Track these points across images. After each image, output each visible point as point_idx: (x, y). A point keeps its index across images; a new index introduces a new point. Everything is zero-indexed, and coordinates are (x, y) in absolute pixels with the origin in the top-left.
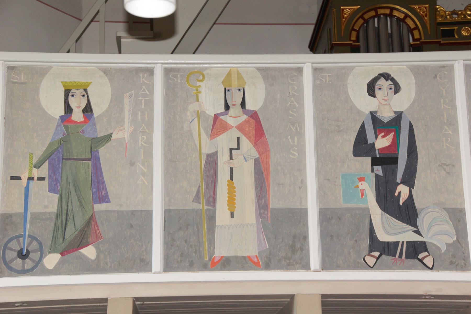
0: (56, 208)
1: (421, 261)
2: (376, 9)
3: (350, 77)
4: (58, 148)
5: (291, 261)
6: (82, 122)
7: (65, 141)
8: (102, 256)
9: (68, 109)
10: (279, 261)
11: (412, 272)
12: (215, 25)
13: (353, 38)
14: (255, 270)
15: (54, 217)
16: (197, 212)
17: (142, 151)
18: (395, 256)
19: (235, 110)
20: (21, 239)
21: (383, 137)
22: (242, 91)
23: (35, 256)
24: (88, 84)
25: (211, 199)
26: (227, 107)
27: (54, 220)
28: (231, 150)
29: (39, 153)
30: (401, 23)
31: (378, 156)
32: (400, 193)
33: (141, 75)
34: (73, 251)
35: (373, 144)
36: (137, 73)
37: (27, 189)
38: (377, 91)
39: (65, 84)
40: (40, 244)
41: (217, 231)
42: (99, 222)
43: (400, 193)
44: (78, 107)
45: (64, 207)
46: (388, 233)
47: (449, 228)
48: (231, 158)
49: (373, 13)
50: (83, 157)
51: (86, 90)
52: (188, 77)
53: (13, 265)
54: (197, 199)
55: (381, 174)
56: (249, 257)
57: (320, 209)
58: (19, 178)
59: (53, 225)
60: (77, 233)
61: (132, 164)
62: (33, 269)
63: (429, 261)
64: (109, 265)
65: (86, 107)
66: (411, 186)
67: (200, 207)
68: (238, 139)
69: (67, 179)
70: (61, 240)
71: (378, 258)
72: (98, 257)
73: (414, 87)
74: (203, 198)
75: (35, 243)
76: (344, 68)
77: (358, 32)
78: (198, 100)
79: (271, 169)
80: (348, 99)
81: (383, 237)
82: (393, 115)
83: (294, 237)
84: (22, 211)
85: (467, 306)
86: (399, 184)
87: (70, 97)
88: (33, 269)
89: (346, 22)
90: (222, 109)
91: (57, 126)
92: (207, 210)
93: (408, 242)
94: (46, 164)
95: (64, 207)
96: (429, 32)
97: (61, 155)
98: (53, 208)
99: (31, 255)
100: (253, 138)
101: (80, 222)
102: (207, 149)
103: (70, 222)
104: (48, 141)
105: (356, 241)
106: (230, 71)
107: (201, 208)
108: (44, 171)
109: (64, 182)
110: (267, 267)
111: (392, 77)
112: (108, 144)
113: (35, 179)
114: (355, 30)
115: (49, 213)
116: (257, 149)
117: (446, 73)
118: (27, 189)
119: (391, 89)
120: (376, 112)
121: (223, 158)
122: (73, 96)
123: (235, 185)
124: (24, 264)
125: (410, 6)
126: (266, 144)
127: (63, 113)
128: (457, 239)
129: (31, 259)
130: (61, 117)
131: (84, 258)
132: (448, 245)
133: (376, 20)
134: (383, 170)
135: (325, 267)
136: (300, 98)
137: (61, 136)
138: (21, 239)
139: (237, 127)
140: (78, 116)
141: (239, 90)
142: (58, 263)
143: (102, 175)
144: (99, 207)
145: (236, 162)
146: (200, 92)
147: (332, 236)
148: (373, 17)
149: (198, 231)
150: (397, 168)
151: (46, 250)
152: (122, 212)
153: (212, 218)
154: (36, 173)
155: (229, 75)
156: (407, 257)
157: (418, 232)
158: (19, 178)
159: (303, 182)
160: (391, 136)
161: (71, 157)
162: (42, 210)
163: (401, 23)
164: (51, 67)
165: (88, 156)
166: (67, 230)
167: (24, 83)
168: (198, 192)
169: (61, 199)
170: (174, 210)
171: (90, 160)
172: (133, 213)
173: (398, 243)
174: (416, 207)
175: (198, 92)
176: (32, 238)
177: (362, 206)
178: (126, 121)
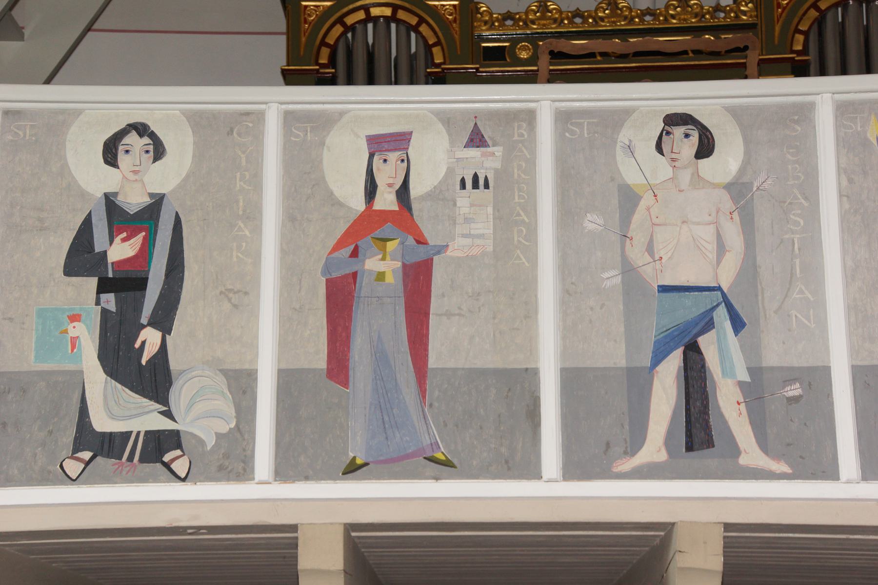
1: (167, 466)
18: (120, 458)
21: (124, 240)
22: (406, 161)
32: (143, 343)
35: (105, 253)
43: (143, 343)
47: (226, 406)
63: (181, 467)
71: (87, 463)
81: (102, 423)
82: (147, 200)
86: (144, 327)
111: (152, 131)
117: (251, 125)
119: (147, 152)
120: (116, 194)
132: (219, 436)
150: (144, 296)
156: (142, 460)
157: (168, 414)
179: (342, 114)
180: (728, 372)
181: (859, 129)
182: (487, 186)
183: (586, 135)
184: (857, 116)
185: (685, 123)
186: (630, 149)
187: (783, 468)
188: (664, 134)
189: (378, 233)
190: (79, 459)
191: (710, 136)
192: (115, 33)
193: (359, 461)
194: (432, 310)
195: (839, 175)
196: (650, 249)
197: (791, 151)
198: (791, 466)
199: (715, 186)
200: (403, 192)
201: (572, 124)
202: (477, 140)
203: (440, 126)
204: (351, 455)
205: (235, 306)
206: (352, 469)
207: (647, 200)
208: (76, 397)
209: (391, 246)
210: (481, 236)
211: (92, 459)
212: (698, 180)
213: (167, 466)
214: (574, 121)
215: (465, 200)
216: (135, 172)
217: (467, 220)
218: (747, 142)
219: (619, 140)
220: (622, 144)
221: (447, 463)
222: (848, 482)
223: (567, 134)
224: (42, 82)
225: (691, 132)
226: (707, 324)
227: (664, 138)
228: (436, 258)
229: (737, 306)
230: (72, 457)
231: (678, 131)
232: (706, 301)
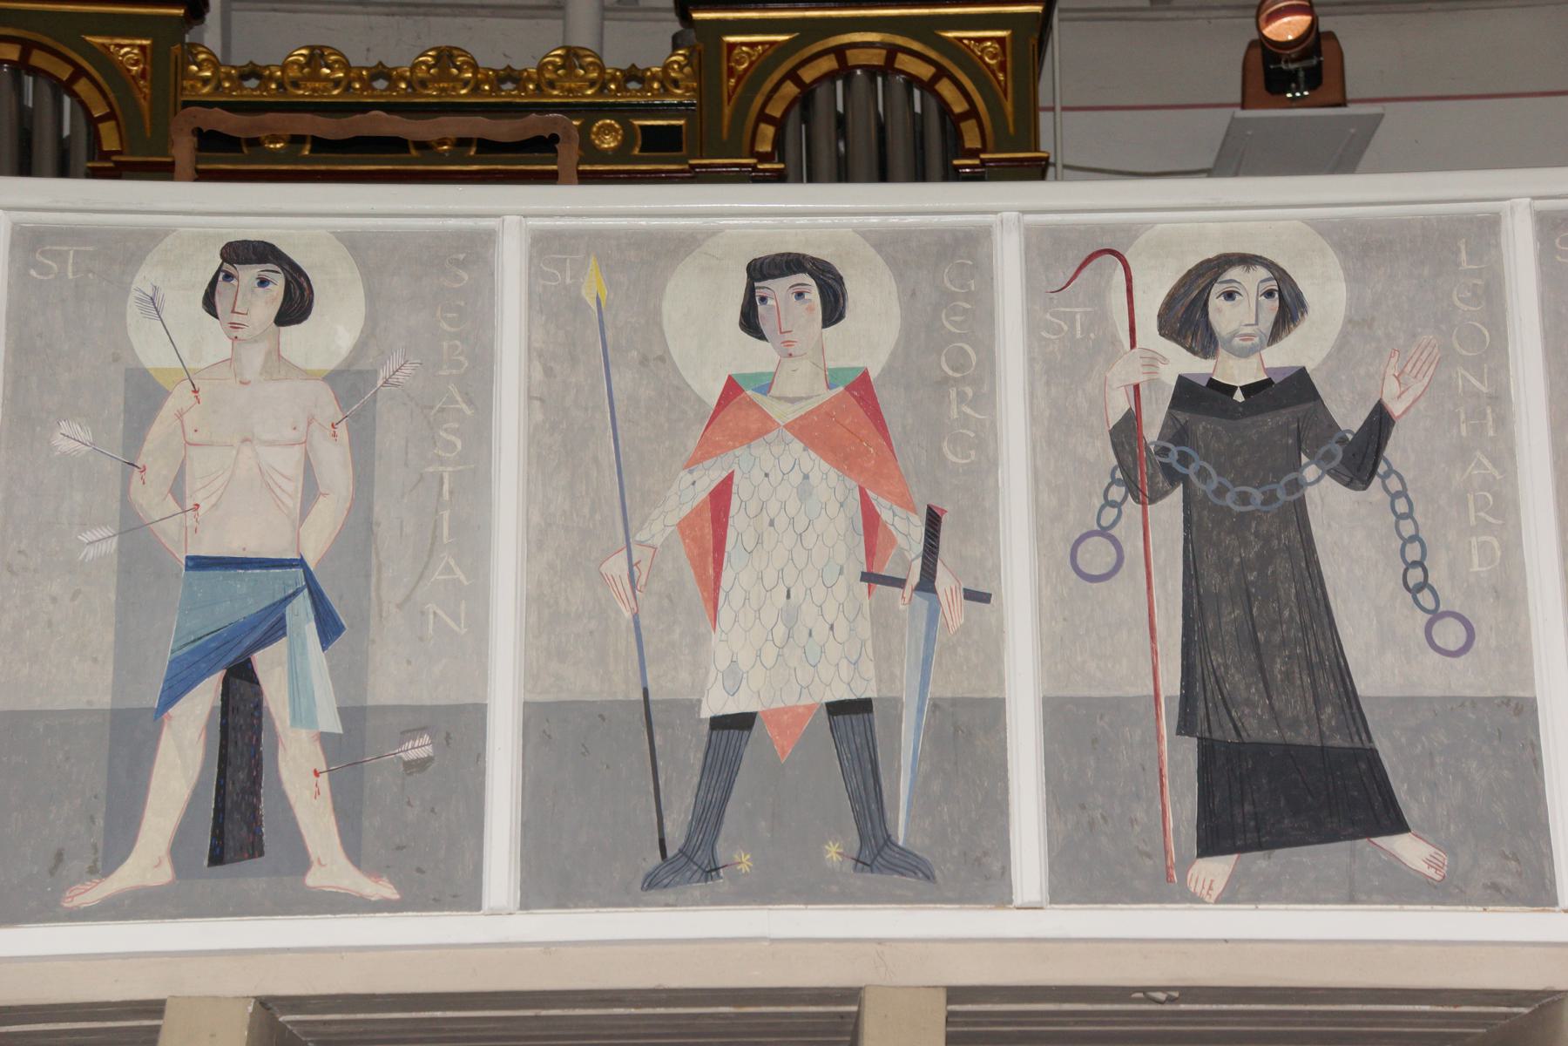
11: (431, 916)
13: (765, 147)
57: (526, 704)
77: (780, 124)
85: (1544, 1002)
89: (739, 90)
96: (725, 130)
114: (770, 120)
125: (88, 38)
133: (839, 84)
148: (830, 77)
174: (1359, 693)
181: (568, 281)
183: (70, 276)
184: (566, 259)
185: (261, 260)
186: (153, 303)
188: (221, 275)
191: (305, 284)
195: (530, 360)
196: (177, 489)
197: (449, 315)
198: (398, 886)
201: (43, 253)
212: (277, 364)
214: (48, 248)
218: (371, 296)
219: (134, 286)
220: (138, 294)
223: (33, 273)
225: (270, 276)
227: (221, 285)
231: (248, 274)
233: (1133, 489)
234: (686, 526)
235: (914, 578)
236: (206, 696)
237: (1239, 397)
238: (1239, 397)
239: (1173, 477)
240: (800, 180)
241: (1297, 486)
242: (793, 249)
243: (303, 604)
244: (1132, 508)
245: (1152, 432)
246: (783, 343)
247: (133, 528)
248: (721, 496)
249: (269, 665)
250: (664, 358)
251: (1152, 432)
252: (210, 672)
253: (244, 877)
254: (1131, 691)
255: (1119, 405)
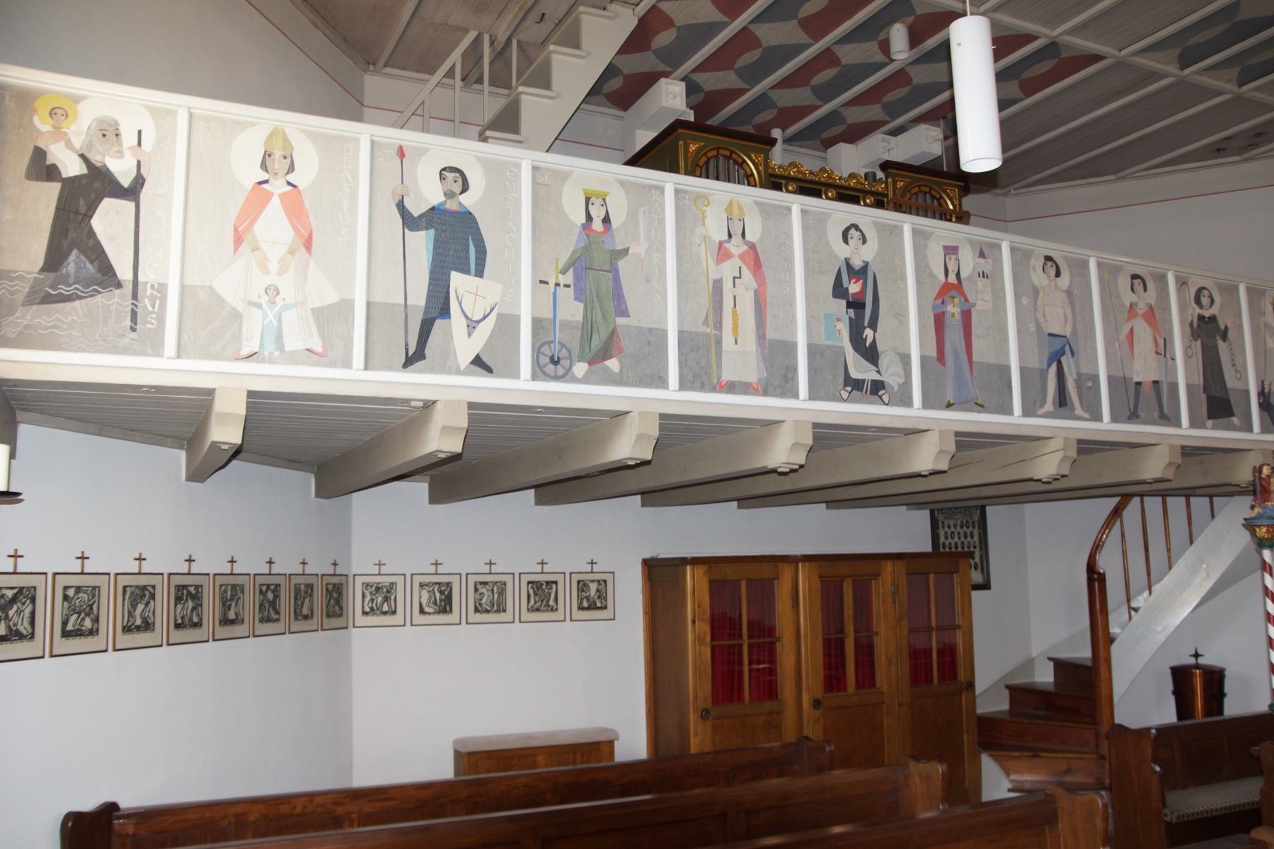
0: (582, 317)
1: (880, 397)
2: (717, 149)
3: (829, 223)
4: (580, 256)
5: (784, 390)
6: (601, 232)
7: (587, 250)
8: (625, 370)
9: (589, 218)
10: (775, 389)
12: (557, 141)
14: (755, 395)
15: (580, 326)
16: (707, 335)
17: (657, 269)
18: (862, 391)
19: (737, 239)
20: (552, 345)
21: (855, 283)
23: (565, 363)
24: (606, 194)
25: (718, 325)
26: (730, 236)
27: (580, 329)
28: (734, 278)
29: (564, 258)
30: (736, 167)
31: (851, 300)
32: (866, 336)
33: (653, 192)
34: (599, 362)
35: (847, 289)
36: (650, 190)
37: (555, 294)
38: (850, 240)
39: (585, 191)
40: (569, 352)
41: (724, 355)
42: (620, 336)
43: (866, 336)
44: (598, 217)
45: (589, 317)
46: (858, 371)
47: (899, 369)
48: (734, 286)
49: (714, 153)
50: (604, 269)
51: (604, 200)
52: (695, 201)
53: (546, 370)
54: (706, 323)
55: (853, 317)
56: (750, 383)
58: (546, 283)
59: (579, 333)
60: (601, 344)
61: (648, 281)
62: (564, 376)
63: (886, 398)
64: (631, 379)
65: (605, 217)
66: (875, 331)
67: (709, 330)
68: (740, 268)
69: (590, 288)
70: (588, 350)
71: (850, 393)
72: (621, 370)
73: (876, 240)
74: (711, 322)
75: (564, 350)
76: (823, 213)
78: (704, 224)
79: (768, 300)
80: (827, 243)
81: (854, 374)
82: (861, 264)
83: (787, 368)
84: (552, 317)
86: (866, 328)
87: (590, 204)
88: (564, 376)
90: (726, 237)
91: (580, 233)
92: (715, 334)
93: (872, 381)
94: (571, 272)
95: (589, 317)
97: (584, 264)
98: (579, 317)
99: (562, 362)
100: (752, 269)
101: (604, 333)
102: (714, 275)
103: (595, 332)
104: (572, 249)
105: (834, 376)
106: (731, 200)
107: (710, 331)
108: (569, 278)
109: (588, 292)
110: (765, 394)
112: (626, 258)
113: (562, 285)
115: (576, 322)
116: (756, 280)
118: (555, 294)
120: (849, 259)
121: (727, 285)
122: (593, 204)
123: (738, 313)
124: (556, 370)
126: (763, 276)
127: (584, 221)
128: (905, 381)
129: (562, 366)
130: (582, 224)
131: (607, 370)
132: (899, 385)
134: (855, 313)
135: (813, 396)
136: (789, 235)
137: (583, 244)
138: (552, 345)
139: (739, 256)
140: (597, 225)
141: (740, 220)
142: (587, 373)
143: (621, 289)
144: (620, 321)
145: (740, 290)
146: (706, 217)
147: (816, 370)
149: (708, 354)
150: (865, 312)
151: (575, 358)
152: (641, 328)
153: (719, 343)
154: (562, 279)
155: (731, 203)
156: (871, 394)
157: (878, 372)
158: (546, 283)
159: (794, 317)
160: (860, 283)
161: (593, 267)
162: (569, 318)
163: (736, 167)
164: (572, 172)
165: (607, 267)
166: (592, 340)
167: (548, 185)
168: (707, 315)
169: (586, 307)
170: (687, 331)
171: (610, 272)
172: (651, 330)
173: (864, 380)
175: (704, 217)
176: (562, 345)
177: (838, 344)
178: (642, 236)
179: (932, 233)
180: (1071, 375)
182: (987, 277)
186: (1034, 268)
187: (1087, 416)
189: (950, 294)
190: (846, 391)
192: (562, 128)
193: (951, 402)
194: (973, 334)
196: (1044, 316)
198: (1091, 415)
199: (1062, 291)
200: (958, 275)
202: (982, 255)
203: (969, 246)
204: (948, 399)
205: (900, 322)
206: (949, 406)
207: (1041, 294)
208: (843, 360)
209: (956, 300)
210: (987, 301)
211: (852, 391)
212: (1057, 287)
213: (880, 397)
215: (981, 282)
216: (856, 249)
217: (982, 293)
221: (981, 406)
222: (168, 358)
224: (624, 162)
226: (1064, 353)
228: (972, 309)
229: (1072, 346)
230: (844, 390)
232: (1063, 341)
233: (1194, 338)
234: (1127, 336)
235: (1163, 354)
236: (1053, 368)
237: (1207, 319)
238: (1207, 319)
239: (1199, 336)
240: (735, 183)
241: (1216, 341)
242: (1137, 273)
243: (1067, 348)
244: (1193, 342)
245: (1195, 325)
246: (101, 130)
247: (1038, 324)
248: (1132, 329)
249: (1063, 359)
250: (1120, 296)
251: (1195, 325)
252: (1054, 361)
253: (1063, 411)
254: (1196, 383)
255: (1190, 319)
